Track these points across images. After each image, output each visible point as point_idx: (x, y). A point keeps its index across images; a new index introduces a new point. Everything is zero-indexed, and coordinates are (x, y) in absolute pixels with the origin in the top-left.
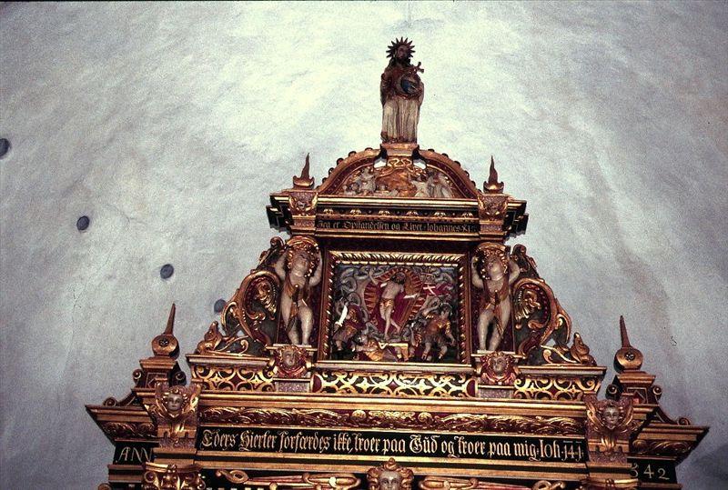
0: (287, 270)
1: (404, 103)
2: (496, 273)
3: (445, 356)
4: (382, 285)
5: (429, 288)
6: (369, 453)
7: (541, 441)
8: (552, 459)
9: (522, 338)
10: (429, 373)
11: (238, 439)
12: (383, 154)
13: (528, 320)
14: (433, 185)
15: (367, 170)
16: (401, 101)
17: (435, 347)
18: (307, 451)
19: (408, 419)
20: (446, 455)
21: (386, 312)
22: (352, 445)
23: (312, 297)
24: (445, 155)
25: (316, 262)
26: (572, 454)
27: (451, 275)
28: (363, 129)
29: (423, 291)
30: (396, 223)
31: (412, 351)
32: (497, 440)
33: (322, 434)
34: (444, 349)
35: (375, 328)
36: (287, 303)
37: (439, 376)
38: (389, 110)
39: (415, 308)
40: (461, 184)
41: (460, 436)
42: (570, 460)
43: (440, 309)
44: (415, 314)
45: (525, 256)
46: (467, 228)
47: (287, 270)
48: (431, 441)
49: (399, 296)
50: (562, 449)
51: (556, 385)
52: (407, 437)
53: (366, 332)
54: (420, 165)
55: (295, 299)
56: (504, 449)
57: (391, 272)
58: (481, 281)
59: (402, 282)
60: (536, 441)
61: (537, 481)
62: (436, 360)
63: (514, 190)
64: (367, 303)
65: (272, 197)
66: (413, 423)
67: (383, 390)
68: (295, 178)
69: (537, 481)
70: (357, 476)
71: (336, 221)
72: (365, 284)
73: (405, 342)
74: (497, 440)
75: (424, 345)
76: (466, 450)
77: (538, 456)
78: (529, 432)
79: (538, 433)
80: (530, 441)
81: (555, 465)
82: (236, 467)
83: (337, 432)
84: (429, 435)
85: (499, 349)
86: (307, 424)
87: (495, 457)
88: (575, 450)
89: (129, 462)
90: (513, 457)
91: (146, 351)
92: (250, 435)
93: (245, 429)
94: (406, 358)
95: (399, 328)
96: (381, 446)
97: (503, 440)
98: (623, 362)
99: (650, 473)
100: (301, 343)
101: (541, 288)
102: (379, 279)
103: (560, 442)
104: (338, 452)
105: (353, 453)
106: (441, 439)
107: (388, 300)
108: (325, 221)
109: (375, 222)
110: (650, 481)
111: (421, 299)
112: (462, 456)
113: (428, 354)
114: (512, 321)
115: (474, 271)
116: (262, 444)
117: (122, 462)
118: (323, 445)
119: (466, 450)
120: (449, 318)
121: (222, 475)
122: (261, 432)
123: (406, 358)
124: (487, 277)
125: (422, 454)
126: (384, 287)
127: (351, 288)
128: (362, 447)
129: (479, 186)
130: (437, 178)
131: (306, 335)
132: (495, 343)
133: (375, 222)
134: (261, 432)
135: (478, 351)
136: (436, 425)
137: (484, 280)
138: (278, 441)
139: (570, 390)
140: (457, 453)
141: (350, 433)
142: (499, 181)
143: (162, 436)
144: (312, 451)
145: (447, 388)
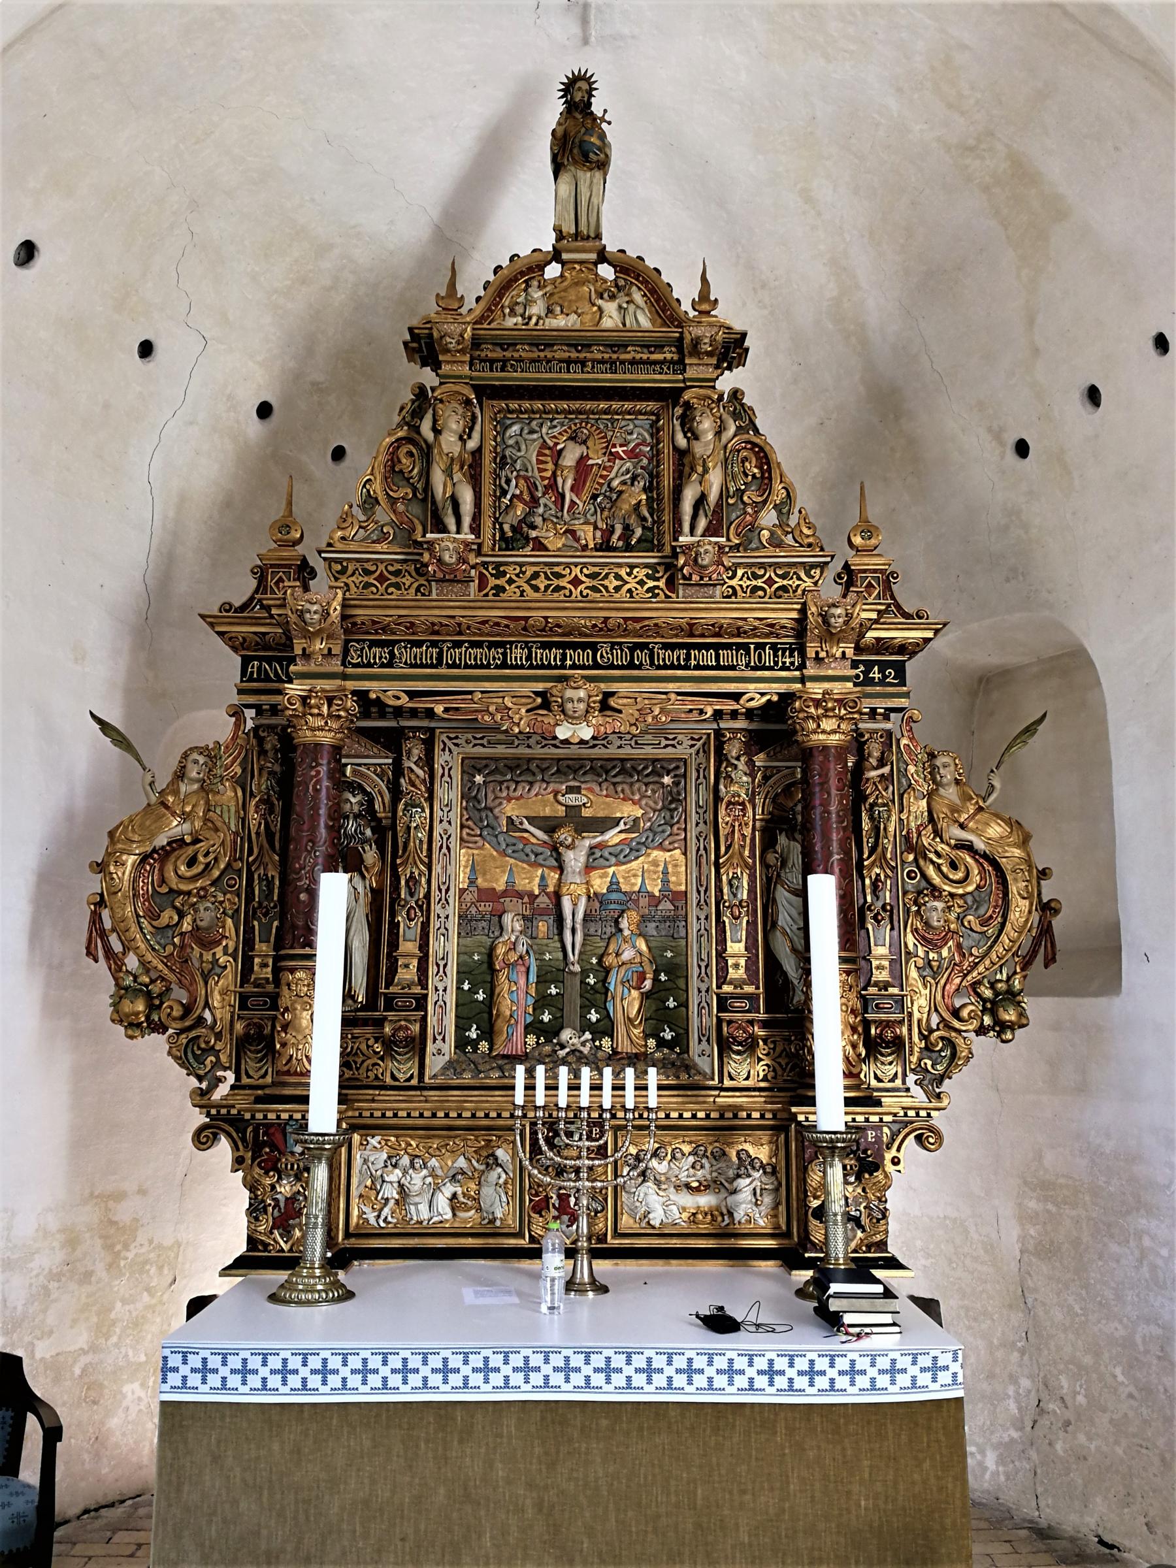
0: (437, 432)
1: (585, 176)
2: (706, 432)
3: (639, 541)
4: (559, 447)
5: (619, 450)
6: (549, 667)
7: (752, 646)
8: (764, 668)
9: (734, 516)
10: (620, 565)
11: (392, 654)
12: (556, 256)
13: (743, 492)
14: (625, 305)
15: (535, 283)
16: (580, 174)
17: (628, 530)
18: (476, 667)
19: (595, 626)
20: (639, 667)
21: (566, 483)
22: (529, 658)
23: (470, 466)
24: (639, 258)
25: (474, 418)
26: (788, 660)
27: (647, 431)
28: (526, 217)
29: (611, 453)
30: (576, 362)
31: (598, 534)
32: (700, 647)
33: (492, 645)
34: (639, 532)
35: (553, 507)
36: (438, 478)
37: (632, 567)
38: (565, 188)
39: (601, 476)
40: (659, 297)
41: (656, 643)
42: (784, 668)
43: (634, 478)
44: (601, 485)
45: (743, 405)
46: (669, 368)
47: (437, 432)
48: (622, 651)
49: (582, 459)
50: (776, 655)
51: (773, 575)
52: (594, 647)
53: (541, 510)
54: (606, 271)
55: (449, 473)
56: (709, 658)
57: (570, 428)
58: (685, 441)
59: (584, 442)
60: (745, 647)
61: (745, 693)
62: (628, 548)
63: (731, 312)
64: (540, 470)
65: (411, 330)
66: (601, 629)
67: (565, 588)
68: (438, 295)
69: (745, 693)
70: (537, 694)
71: (499, 361)
72: (537, 444)
73: (590, 524)
74: (700, 647)
75: (613, 526)
76: (664, 660)
77: (747, 666)
78: (739, 636)
79: (748, 637)
80: (739, 646)
81: (767, 674)
82: (395, 687)
83: (511, 643)
84: (620, 644)
85: (708, 532)
86: (475, 634)
87: (698, 667)
88: (791, 656)
89: (258, 680)
90: (718, 667)
91: (266, 545)
92: (405, 648)
93: (400, 641)
94: (591, 545)
95: (581, 505)
96: (564, 659)
97: (707, 647)
98: (857, 540)
99: (877, 675)
100: (458, 532)
101: (762, 449)
102: (554, 437)
103: (774, 647)
104: (512, 667)
105: (531, 667)
106: (634, 647)
107: (567, 467)
108: (481, 361)
109: (549, 361)
110: (876, 684)
111: (608, 464)
112: (659, 667)
113: (619, 539)
114: (724, 493)
115: (678, 428)
116: (421, 659)
117: (251, 680)
118: (494, 659)
119: (664, 660)
120: (645, 490)
121: (378, 698)
122: (418, 644)
123: (591, 545)
124: (693, 435)
125: (612, 667)
126: (562, 450)
127: (519, 450)
128: (541, 659)
129: (686, 306)
130: (628, 295)
131: (467, 521)
132: (702, 523)
133: (549, 361)
134: (418, 644)
135: (681, 539)
136: (626, 632)
137: (688, 439)
138: (440, 654)
139: (790, 582)
140: (652, 663)
141: (527, 643)
142: (712, 298)
143: (300, 652)
144: (482, 667)
145: (642, 583)
